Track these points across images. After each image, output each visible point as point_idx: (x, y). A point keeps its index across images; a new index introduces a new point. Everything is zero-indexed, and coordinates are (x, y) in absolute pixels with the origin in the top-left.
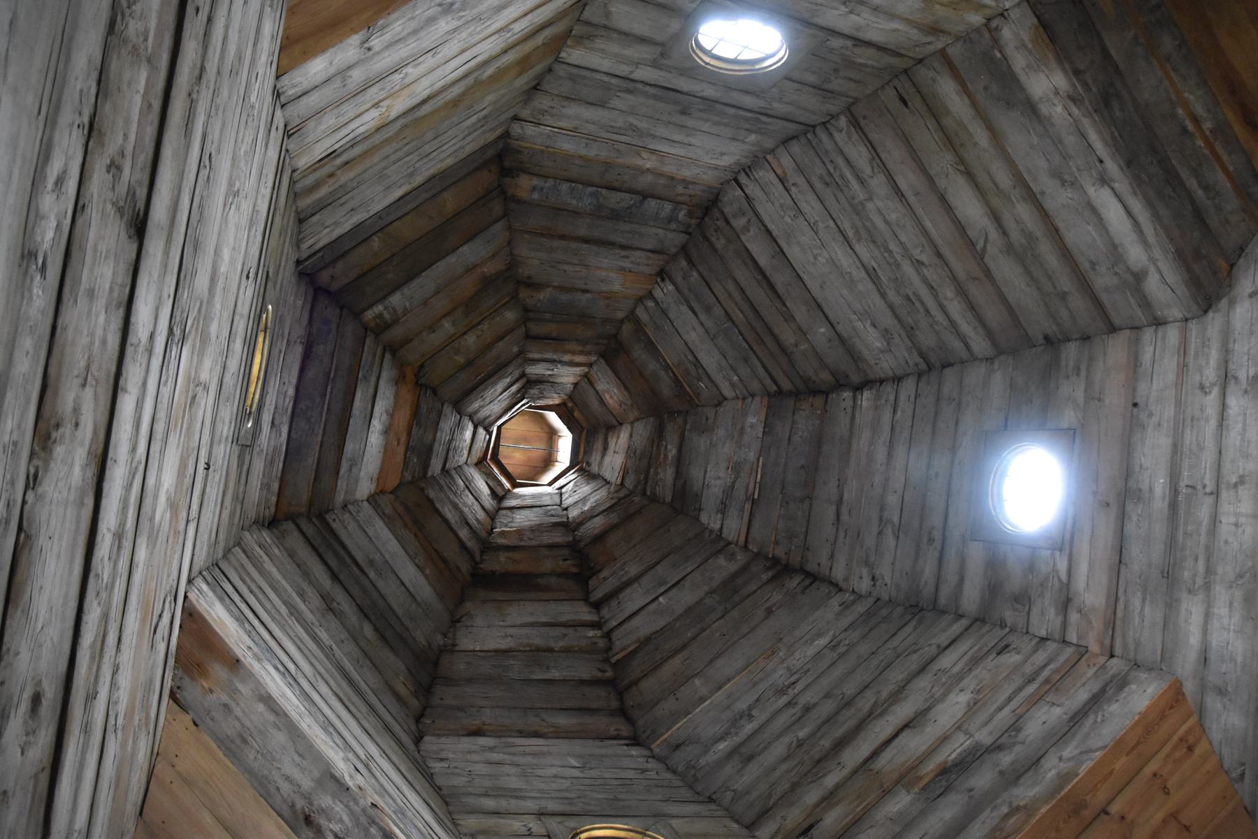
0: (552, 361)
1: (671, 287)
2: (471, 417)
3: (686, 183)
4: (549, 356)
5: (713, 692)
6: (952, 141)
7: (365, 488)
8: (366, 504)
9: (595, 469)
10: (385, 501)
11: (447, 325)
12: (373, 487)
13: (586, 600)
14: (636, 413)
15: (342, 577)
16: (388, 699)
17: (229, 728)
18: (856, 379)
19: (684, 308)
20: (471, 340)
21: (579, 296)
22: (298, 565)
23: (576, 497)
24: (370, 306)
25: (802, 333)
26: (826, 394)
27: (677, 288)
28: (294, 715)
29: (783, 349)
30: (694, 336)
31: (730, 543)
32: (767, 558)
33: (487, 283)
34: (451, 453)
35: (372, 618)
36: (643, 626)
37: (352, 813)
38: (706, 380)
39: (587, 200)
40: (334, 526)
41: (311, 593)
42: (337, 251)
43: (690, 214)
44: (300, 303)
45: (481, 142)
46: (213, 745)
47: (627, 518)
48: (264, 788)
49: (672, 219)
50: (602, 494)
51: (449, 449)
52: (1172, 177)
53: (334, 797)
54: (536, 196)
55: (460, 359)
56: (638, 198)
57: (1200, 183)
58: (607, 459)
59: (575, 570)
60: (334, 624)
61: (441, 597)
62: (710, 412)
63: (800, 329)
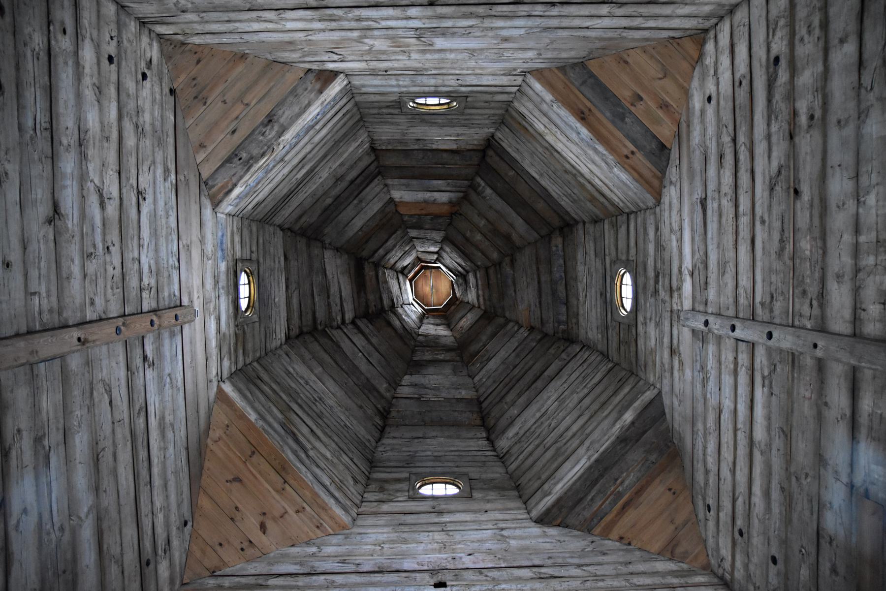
0: (477, 285)
1: (526, 335)
2: (441, 248)
3: (577, 323)
4: (480, 283)
5: (316, 375)
7: (397, 195)
8: (389, 197)
9: (425, 321)
10: (391, 208)
11: (483, 223)
12: (397, 200)
13: (356, 317)
14: (458, 336)
15: (353, 186)
16: (298, 212)
17: (300, 91)
19: (516, 344)
20: (479, 237)
21: (512, 288)
22: (355, 163)
23: (409, 312)
24: (482, 179)
25: (513, 403)
26: (483, 426)
27: (526, 337)
28: (304, 116)
29: (503, 397)
30: (503, 354)
31: (395, 390)
32: (389, 408)
33: (508, 238)
34: (421, 240)
36: (346, 345)
37: (272, 139)
38: (481, 366)
39: (557, 275)
40: (376, 180)
41: (344, 169)
42: (502, 154)
43: (564, 331)
44: (476, 142)
45: (569, 210)
46: (294, 85)
47: (401, 337)
48: (281, 104)
49: (559, 322)
50: (413, 325)
51: (423, 239)
52: (595, 482)
53: (277, 132)
54: (554, 249)
55: (468, 234)
56: (565, 301)
58: (431, 326)
59: (370, 311)
60: (331, 183)
62: (465, 372)
63: (515, 402)
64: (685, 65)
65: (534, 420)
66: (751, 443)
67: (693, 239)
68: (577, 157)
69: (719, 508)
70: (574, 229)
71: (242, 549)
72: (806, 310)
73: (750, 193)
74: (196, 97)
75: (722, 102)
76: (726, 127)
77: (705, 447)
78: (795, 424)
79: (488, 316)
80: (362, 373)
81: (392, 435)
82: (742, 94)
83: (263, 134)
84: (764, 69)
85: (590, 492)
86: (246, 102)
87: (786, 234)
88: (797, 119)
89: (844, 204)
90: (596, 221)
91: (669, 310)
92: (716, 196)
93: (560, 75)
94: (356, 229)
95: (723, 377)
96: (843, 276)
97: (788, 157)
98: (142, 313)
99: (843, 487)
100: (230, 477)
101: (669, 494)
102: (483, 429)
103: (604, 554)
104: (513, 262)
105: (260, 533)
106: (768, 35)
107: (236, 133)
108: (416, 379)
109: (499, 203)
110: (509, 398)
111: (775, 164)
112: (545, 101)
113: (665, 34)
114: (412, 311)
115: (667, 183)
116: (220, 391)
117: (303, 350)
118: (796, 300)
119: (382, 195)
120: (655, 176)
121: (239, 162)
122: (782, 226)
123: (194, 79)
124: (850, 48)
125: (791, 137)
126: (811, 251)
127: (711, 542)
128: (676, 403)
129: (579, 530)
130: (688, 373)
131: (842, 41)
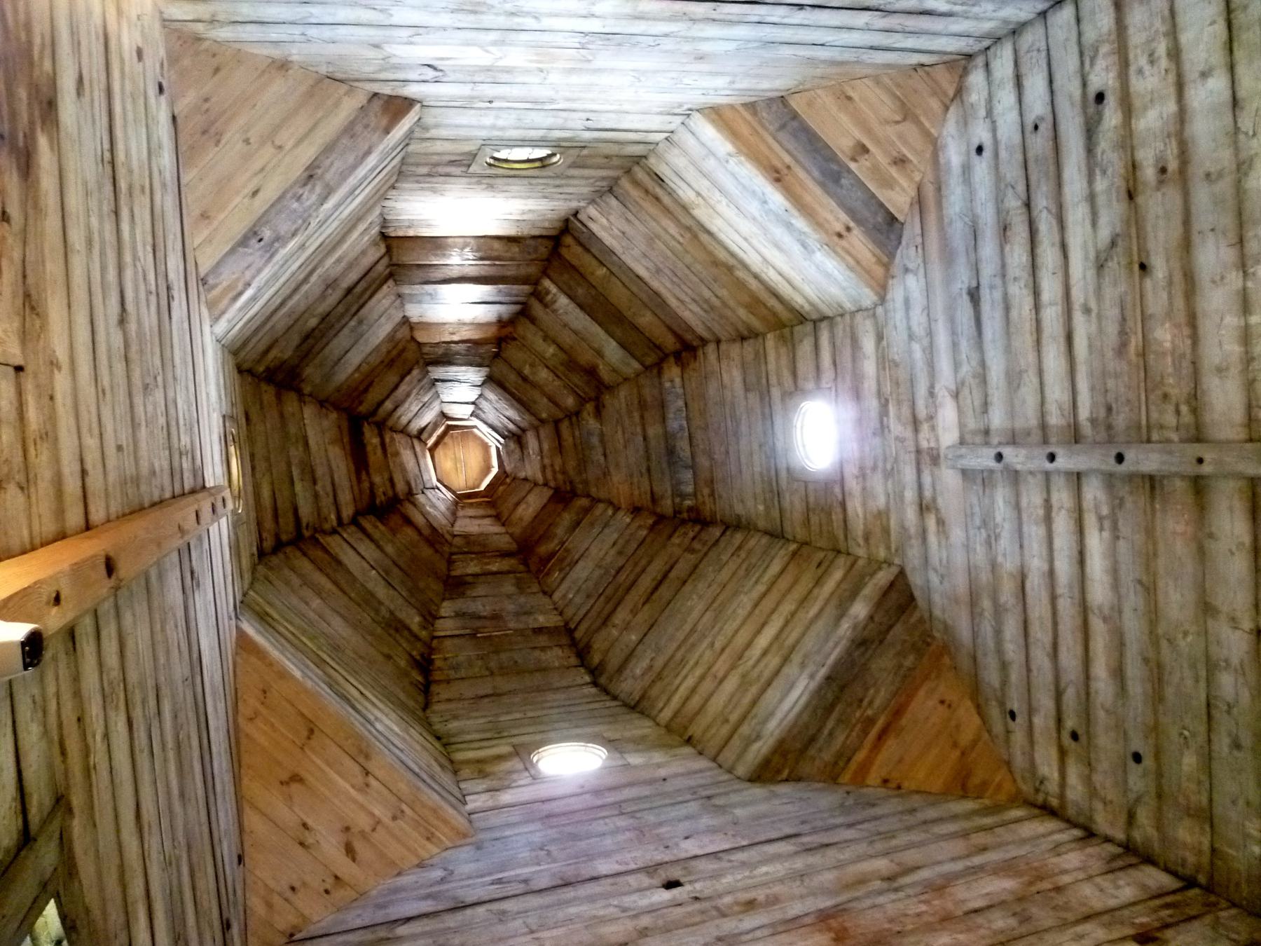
6: (803, 602)
8: (401, 315)
10: (404, 333)
11: (551, 350)
12: (414, 319)
15: (349, 297)
17: (359, 128)
18: (603, 680)
23: (434, 500)
26: (582, 665)
32: (430, 654)
33: (591, 372)
35: (322, 326)
37: (310, 207)
40: (385, 287)
41: (340, 268)
43: (690, 509)
49: (683, 496)
50: (444, 522)
52: (829, 709)
54: (668, 385)
55: (527, 371)
56: (690, 462)
57: (833, 728)
59: (378, 501)
61: (338, 390)
64: (935, 104)
65: (675, 645)
66: (1084, 608)
67: (955, 346)
68: (746, 239)
69: (1031, 711)
70: (700, 353)
71: (327, 892)
72: (1170, 419)
73: (1060, 275)
74: (204, 132)
75: (1003, 154)
76: (1013, 187)
77: (998, 632)
78: (1161, 571)
79: (562, 496)
80: (380, 603)
81: (444, 696)
82: (1040, 144)
83: (299, 198)
84: (1078, 109)
85: (825, 723)
86: (278, 143)
87: (1130, 323)
88: (1138, 173)
89: (1222, 278)
90: (744, 336)
91: (913, 449)
92: (998, 281)
93: (748, 117)
94: (350, 370)
95: (1025, 529)
96: (1227, 369)
97: (1127, 223)
98: (184, 494)
99: (1246, 636)
100: (285, 777)
101: (941, 708)
102: (582, 670)
103: (873, 805)
104: (598, 412)
105: (348, 861)
106: (1082, 63)
107: (260, 195)
108: (460, 604)
109: (579, 320)
110: (621, 616)
111: (1105, 234)
112: (714, 155)
113: (916, 59)
114: (437, 502)
115: (896, 269)
116: (242, 636)
117: (286, 571)
118: (1152, 408)
119: (392, 311)
120: (879, 261)
121: (258, 246)
122: (1123, 315)
123: (206, 100)
124: (1218, 84)
125: (1131, 195)
126: (1173, 342)
127: (1019, 761)
128: (934, 579)
129: (819, 781)
130: (957, 534)
131: (1204, 75)
